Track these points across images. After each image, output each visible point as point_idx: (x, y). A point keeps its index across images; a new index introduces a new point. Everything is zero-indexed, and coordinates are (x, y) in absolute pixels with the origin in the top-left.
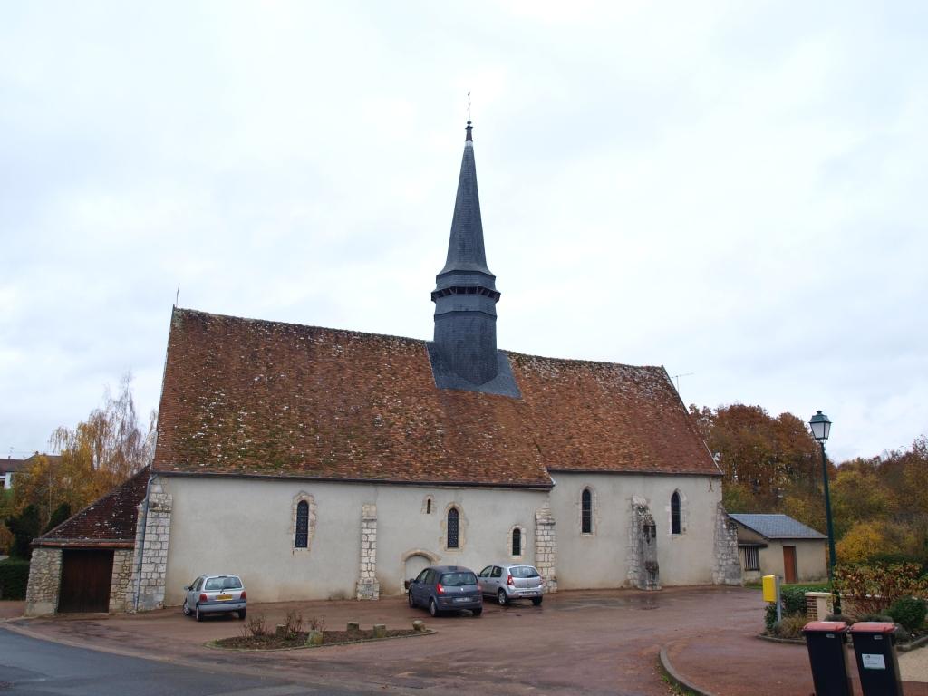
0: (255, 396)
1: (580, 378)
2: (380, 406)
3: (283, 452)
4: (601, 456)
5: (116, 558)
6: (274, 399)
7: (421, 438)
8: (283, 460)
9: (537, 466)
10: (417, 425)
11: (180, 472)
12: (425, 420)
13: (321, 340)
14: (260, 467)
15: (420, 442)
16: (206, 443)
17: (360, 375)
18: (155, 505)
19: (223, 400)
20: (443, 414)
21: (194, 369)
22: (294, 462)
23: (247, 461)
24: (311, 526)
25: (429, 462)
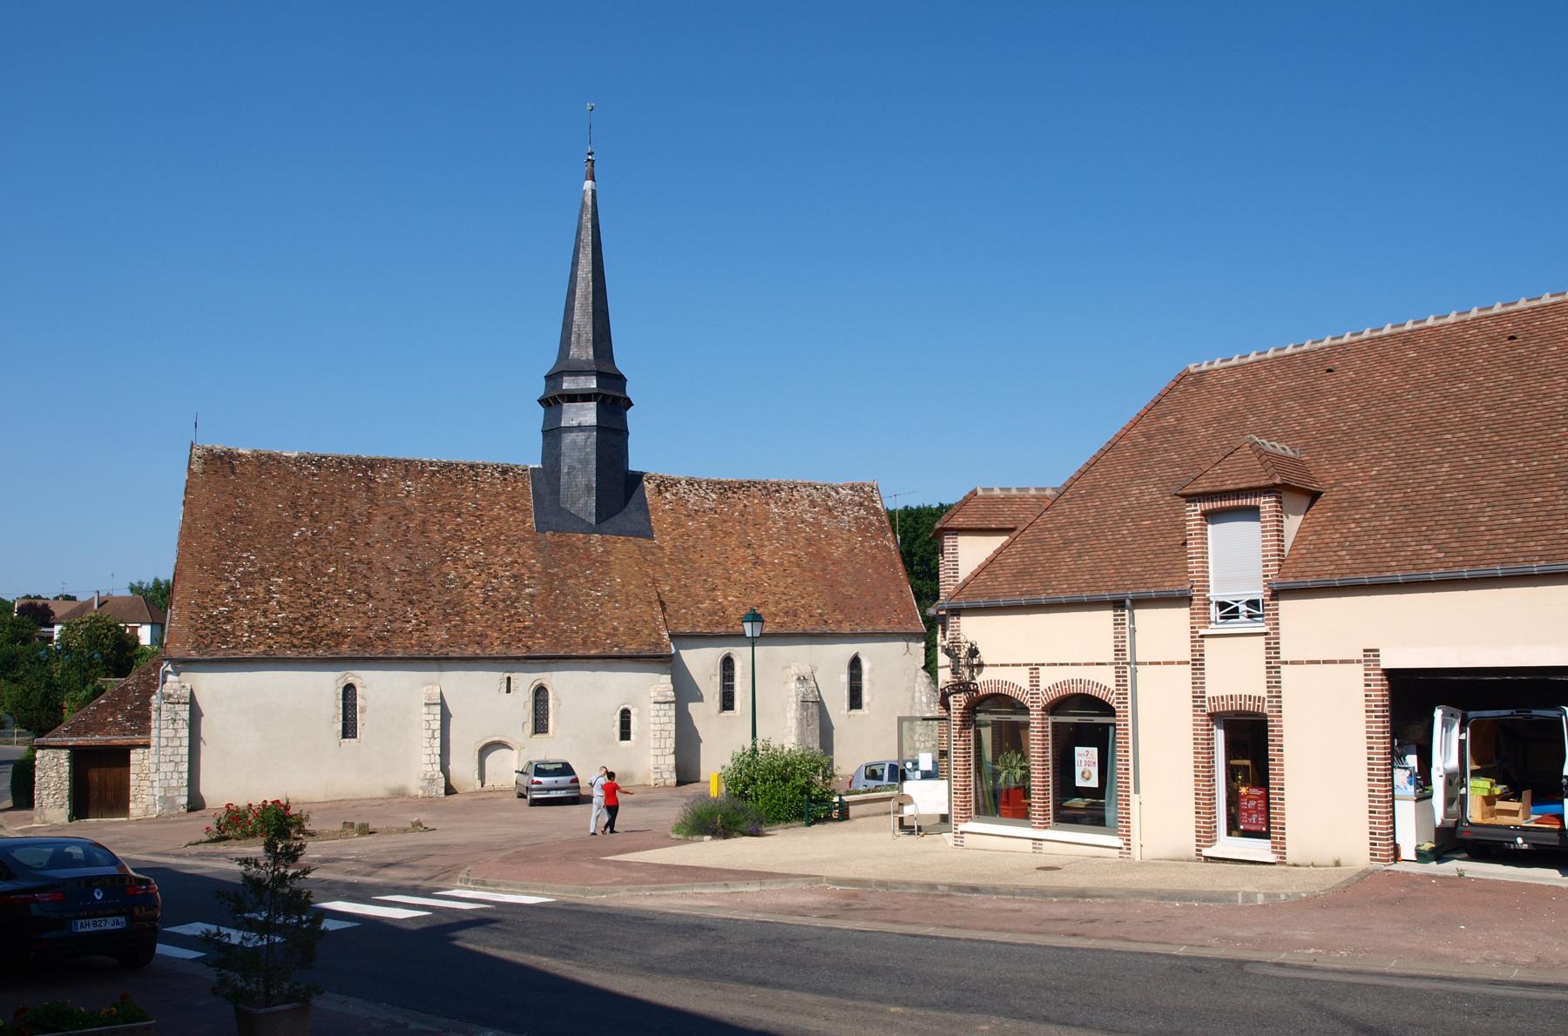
0: (293, 557)
1: (745, 506)
2: (456, 560)
3: (325, 626)
7: (504, 601)
8: (324, 635)
9: (656, 630)
10: (501, 583)
11: (197, 657)
12: (514, 576)
13: (385, 476)
14: (295, 646)
15: (501, 605)
16: (229, 620)
18: (170, 696)
19: (253, 564)
21: (217, 526)
22: (339, 636)
24: (155, 720)
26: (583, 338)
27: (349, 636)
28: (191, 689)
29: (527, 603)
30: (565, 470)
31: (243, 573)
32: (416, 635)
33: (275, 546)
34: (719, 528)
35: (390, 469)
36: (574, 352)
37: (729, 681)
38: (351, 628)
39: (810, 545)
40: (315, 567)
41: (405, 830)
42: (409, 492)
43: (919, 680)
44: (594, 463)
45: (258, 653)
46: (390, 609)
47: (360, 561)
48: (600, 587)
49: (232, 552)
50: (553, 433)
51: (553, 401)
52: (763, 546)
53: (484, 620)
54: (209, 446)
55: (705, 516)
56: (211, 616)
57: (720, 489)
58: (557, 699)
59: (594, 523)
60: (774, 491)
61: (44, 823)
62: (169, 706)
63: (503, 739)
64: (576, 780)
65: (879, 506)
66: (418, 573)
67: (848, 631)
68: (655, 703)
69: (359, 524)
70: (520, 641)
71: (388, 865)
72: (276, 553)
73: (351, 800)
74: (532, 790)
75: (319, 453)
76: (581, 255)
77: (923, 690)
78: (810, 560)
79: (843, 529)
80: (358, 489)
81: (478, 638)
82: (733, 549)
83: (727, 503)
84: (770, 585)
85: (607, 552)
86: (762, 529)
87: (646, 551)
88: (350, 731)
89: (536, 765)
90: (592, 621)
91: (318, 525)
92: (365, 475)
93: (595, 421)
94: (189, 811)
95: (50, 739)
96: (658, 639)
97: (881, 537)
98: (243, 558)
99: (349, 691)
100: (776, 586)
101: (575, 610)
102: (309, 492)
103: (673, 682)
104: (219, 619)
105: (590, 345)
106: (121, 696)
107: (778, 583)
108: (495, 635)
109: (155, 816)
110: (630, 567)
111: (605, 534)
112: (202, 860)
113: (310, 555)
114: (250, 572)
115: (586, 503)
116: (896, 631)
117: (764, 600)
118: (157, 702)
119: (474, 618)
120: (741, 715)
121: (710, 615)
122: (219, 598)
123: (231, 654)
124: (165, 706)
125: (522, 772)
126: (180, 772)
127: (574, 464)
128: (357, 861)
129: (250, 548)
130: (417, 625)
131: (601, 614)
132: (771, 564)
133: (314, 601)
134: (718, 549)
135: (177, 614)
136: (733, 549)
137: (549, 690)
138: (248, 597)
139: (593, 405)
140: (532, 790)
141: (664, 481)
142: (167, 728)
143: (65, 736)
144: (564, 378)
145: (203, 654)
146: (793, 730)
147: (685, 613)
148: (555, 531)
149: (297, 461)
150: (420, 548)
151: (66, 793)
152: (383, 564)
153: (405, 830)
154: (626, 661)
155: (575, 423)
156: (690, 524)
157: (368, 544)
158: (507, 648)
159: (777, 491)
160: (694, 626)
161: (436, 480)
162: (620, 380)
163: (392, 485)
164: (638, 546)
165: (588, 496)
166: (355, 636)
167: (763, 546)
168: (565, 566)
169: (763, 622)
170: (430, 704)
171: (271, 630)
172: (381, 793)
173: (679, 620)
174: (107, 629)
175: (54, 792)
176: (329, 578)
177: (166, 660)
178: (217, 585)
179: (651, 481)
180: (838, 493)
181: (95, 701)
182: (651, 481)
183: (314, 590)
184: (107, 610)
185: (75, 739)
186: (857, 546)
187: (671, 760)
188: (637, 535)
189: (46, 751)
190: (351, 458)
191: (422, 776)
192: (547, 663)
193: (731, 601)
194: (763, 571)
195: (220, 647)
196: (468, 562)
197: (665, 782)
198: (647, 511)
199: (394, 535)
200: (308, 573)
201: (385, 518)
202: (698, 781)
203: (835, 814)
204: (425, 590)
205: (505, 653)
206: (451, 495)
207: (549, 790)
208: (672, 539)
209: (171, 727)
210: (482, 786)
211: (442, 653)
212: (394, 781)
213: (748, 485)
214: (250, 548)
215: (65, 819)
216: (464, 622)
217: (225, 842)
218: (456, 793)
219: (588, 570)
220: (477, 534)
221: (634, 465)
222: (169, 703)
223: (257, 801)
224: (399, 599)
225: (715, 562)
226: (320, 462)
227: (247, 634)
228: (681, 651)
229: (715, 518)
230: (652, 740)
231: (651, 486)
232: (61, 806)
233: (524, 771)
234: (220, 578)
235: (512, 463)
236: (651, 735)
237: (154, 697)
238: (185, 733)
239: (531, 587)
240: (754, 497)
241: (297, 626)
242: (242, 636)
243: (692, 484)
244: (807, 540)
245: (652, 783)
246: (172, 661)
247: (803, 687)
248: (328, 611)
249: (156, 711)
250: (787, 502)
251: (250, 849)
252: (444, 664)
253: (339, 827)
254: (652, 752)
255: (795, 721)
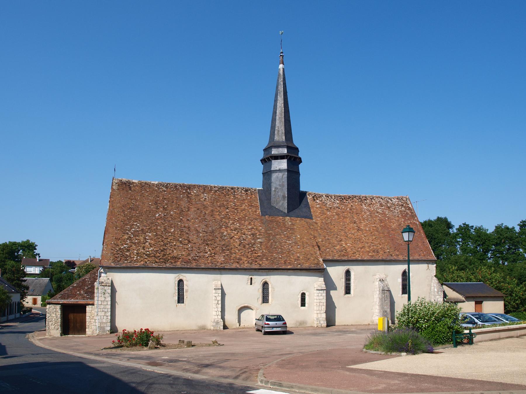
0: (156, 225)
1: (352, 206)
2: (227, 227)
3: (170, 254)
4: (359, 251)
5: (87, 309)
6: (166, 225)
7: (248, 244)
8: (169, 258)
9: (317, 258)
10: (247, 237)
11: (114, 266)
12: (253, 234)
13: (195, 192)
14: (157, 262)
15: (247, 246)
16: (128, 250)
18: (102, 282)
19: (139, 227)
20: (263, 230)
21: (123, 211)
22: (176, 258)
23: (150, 259)
24: (96, 293)
25: (251, 257)
26: (280, 132)
27: (180, 258)
28: (112, 280)
29: (259, 245)
30: (273, 189)
31: (134, 231)
32: (210, 258)
33: (148, 220)
34: (341, 215)
35: (197, 189)
36: (276, 138)
37: (348, 281)
38: (181, 255)
39: (381, 222)
40: (166, 229)
41: (210, 345)
42: (205, 198)
43: (433, 281)
44: (287, 186)
45: (141, 265)
46: (198, 247)
47: (185, 227)
48: (290, 239)
49: (130, 222)
50: (267, 174)
51: (267, 160)
52: (361, 223)
53: (240, 252)
54: (120, 179)
55: (335, 210)
56: (120, 249)
57: (340, 199)
58: (273, 288)
59: (286, 212)
60: (364, 200)
61: (50, 336)
62: (102, 287)
63: (246, 305)
64: (285, 323)
65: (410, 206)
66: (210, 232)
67: (402, 259)
68: (317, 290)
69: (184, 211)
70: (256, 262)
71: (207, 366)
72: (149, 223)
73: (182, 330)
74: (265, 327)
75: (167, 182)
76: (278, 96)
77: (435, 286)
78: (382, 229)
79: (396, 216)
80: (183, 197)
81: (237, 260)
82: (348, 224)
83: (344, 204)
84: (365, 239)
85: (293, 224)
86: (360, 215)
87: (310, 224)
88: (181, 300)
89: (266, 316)
90: (288, 253)
91: (167, 211)
92: (186, 191)
93: (287, 167)
94: (111, 333)
95: (53, 300)
96: (318, 262)
97: (412, 219)
98: (135, 225)
99: (180, 282)
100: (368, 240)
101: (280, 249)
102: (163, 198)
103: (324, 281)
104: (124, 250)
105: (284, 135)
106: (83, 283)
107: (369, 238)
108: (245, 259)
109: (96, 335)
110: (304, 231)
111: (292, 217)
112: (107, 357)
113: (163, 224)
114: (138, 231)
115: (283, 203)
116: (423, 259)
117: (363, 246)
118: (97, 285)
119: (235, 252)
120: (354, 296)
121: (340, 252)
122: (124, 241)
123: (129, 265)
124: (100, 287)
125: (258, 320)
126: (107, 316)
127: (277, 187)
128: (188, 362)
129: (137, 221)
130: (210, 254)
131: (292, 251)
132: (365, 230)
133: (165, 243)
134: (341, 224)
135: (106, 248)
136: (348, 224)
137: (269, 284)
138: (136, 241)
139: (285, 161)
140: (265, 327)
141: (316, 195)
142: (101, 297)
143: (59, 299)
144: (273, 149)
145: (117, 265)
146: (377, 303)
147: (329, 251)
148: (270, 216)
149: (157, 185)
150: (211, 222)
151: (59, 324)
152: (195, 228)
153: (210, 345)
154: (304, 271)
155: (277, 169)
156: (328, 213)
157: (188, 220)
158: (251, 265)
159: (365, 200)
160: (333, 256)
161: (217, 194)
162: (296, 150)
163: (198, 195)
164: (306, 222)
165: (284, 201)
166: (183, 258)
167: (361, 223)
168: (275, 230)
169: (414, 232)
170: (217, 289)
171: (146, 255)
172: (195, 328)
173: (326, 254)
174: (93, 268)
175: (54, 323)
176: (171, 234)
177: (100, 267)
178: (123, 236)
179: (310, 195)
180: (392, 201)
181: (72, 285)
182: (310, 195)
183: (165, 239)
184: (93, 262)
185: (63, 300)
186: (402, 223)
187: (324, 316)
188: (306, 217)
189: (51, 305)
190: (180, 185)
191: (213, 321)
192: (268, 272)
193: (349, 246)
194: (362, 233)
195: (124, 262)
196: (232, 228)
197: (321, 325)
198: (309, 208)
199: (199, 216)
200: (162, 232)
201: (195, 209)
202: (335, 325)
203: (465, 341)
204: (213, 239)
205: (250, 267)
206: (223, 200)
207: (273, 327)
208: (321, 220)
209: (103, 296)
210: (239, 326)
211: (222, 267)
212: (201, 322)
213: (352, 197)
214: (137, 221)
215: (59, 335)
216: (231, 253)
217: (121, 348)
218: (228, 328)
219: (285, 232)
220: (235, 216)
221: (302, 189)
222: (102, 286)
223: (138, 330)
224: (202, 243)
225: (340, 229)
226: (167, 186)
227: (136, 257)
228: (327, 267)
229: (339, 211)
230: (315, 307)
231: (310, 197)
232: (57, 329)
233: (260, 319)
234: (124, 233)
235: (250, 187)
236: (315, 304)
237: (96, 283)
238: (109, 299)
239: (261, 239)
240: (356, 202)
241: (158, 254)
242: (134, 257)
243: (328, 197)
244: (380, 220)
245: (315, 326)
246: (103, 267)
247: (382, 284)
248: (171, 247)
249: (97, 289)
250: (370, 205)
251: (133, 353)
252: (223, 271)
253: (177, 342)
254: (315, 312)
255: (378, 299)
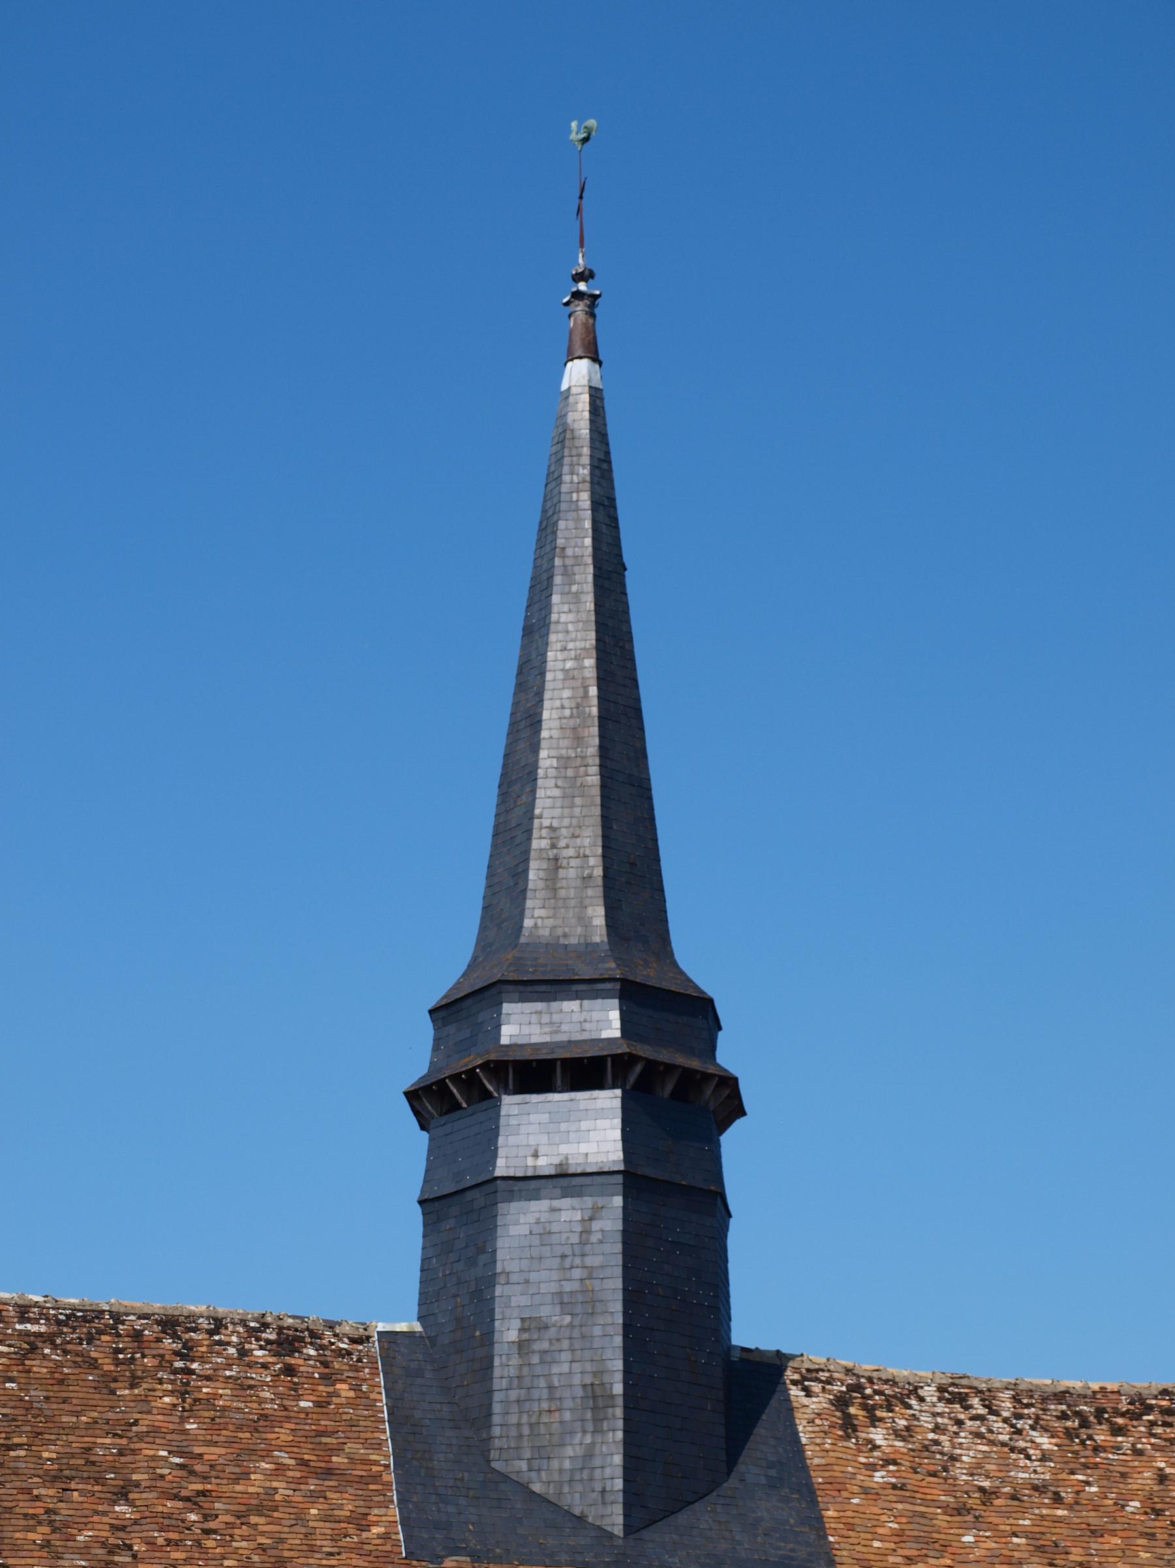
17: (25, 1507)
